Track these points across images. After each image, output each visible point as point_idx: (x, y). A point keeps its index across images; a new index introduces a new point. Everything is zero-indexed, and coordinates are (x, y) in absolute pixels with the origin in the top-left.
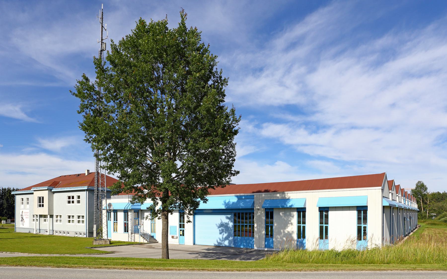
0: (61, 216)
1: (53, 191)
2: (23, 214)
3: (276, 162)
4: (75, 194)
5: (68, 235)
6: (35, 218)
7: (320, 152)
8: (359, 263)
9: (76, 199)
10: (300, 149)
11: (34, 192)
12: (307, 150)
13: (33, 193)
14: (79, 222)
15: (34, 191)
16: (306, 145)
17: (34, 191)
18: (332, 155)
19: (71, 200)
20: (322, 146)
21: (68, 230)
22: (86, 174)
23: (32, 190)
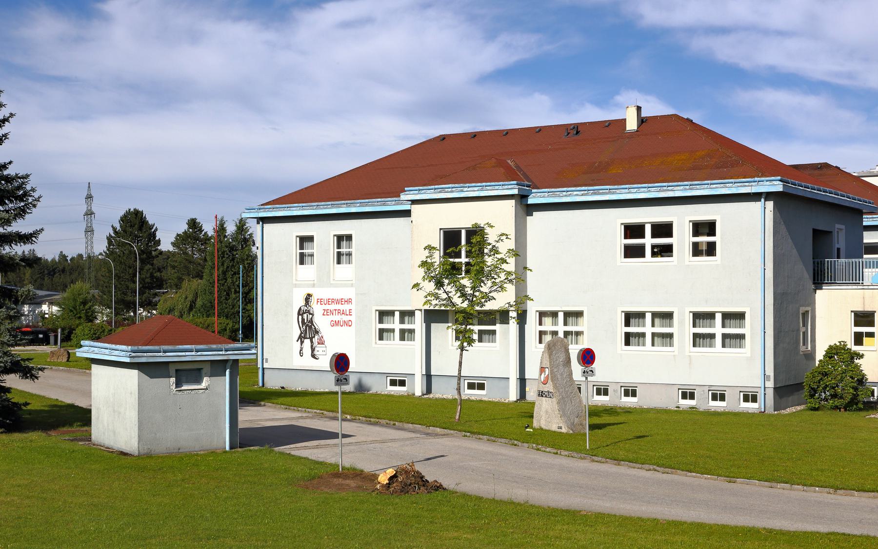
0: (629, 317)
1: (531, 201)
2: (317, 309)
3: (617, 93)
4: (682, 219)
5: (630, 401)
6: (648, 329)
7: (772, 55)
8: (321, 477)
9: (682, 238)
10: (699, 44)
11: (416, 209)
12: (725, 50)
13: (407, 213)
14: (698, 339)
15: (414, 202)
16: (722, 31)
17: (414, 202)
18: (821, 67)
19: (648, 241)
20: (781, 34)
21: (630, 379)
22: (632, 125)
23: (403, 197)
